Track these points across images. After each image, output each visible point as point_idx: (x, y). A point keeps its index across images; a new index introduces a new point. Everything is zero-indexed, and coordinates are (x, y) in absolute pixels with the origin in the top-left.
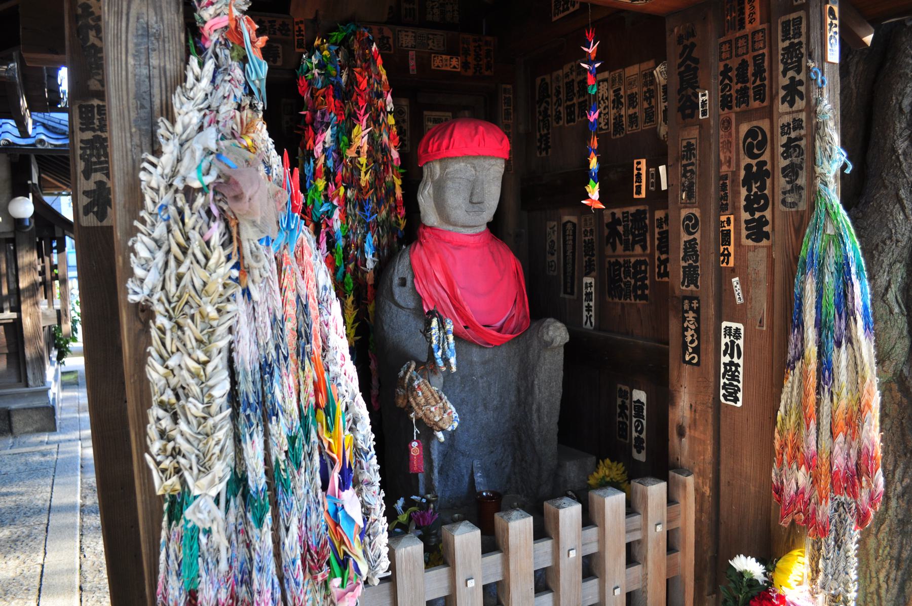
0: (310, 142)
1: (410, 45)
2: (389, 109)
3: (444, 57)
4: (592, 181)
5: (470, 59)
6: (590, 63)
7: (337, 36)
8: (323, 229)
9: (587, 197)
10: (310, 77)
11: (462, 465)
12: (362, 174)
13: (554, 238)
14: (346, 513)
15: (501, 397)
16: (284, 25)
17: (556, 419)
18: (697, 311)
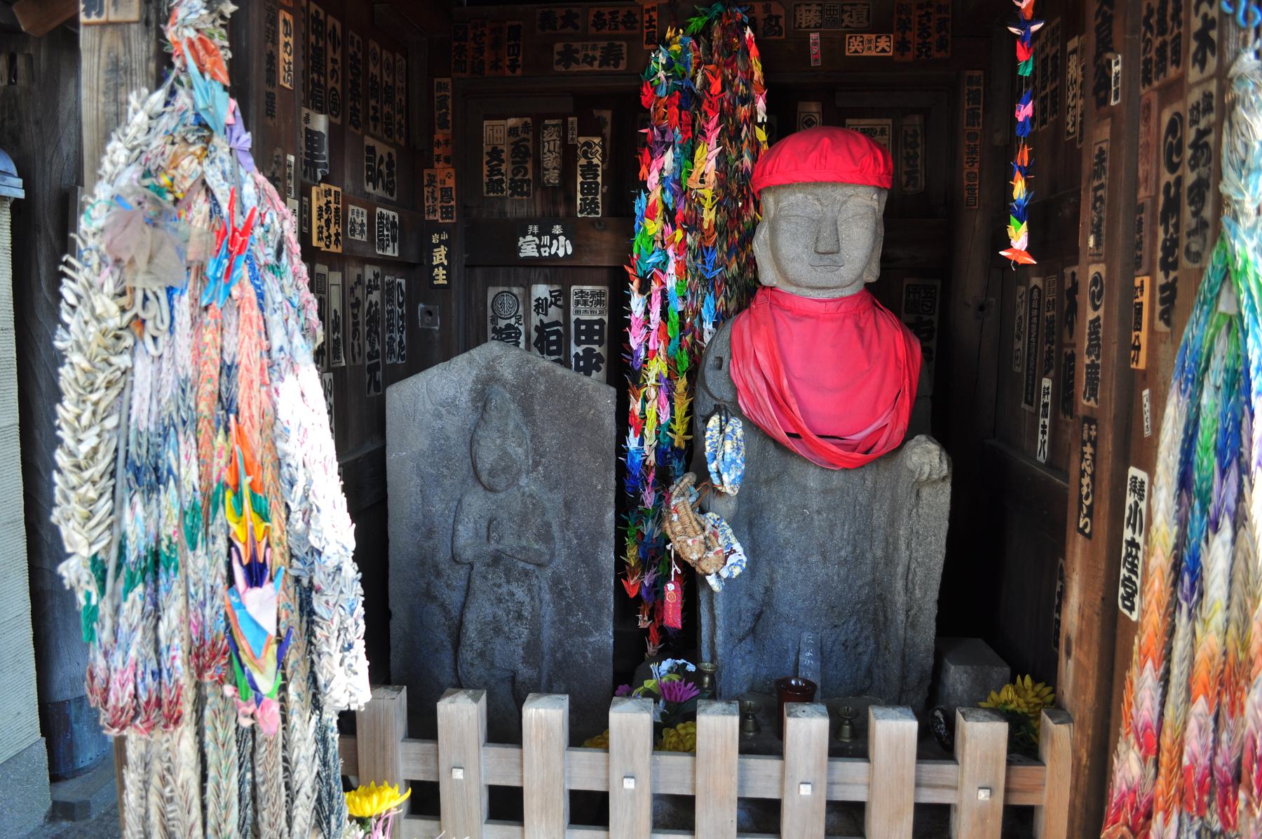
0: (644, 170)
1: (812, 24)
2: (760, 120)
3: (866, 36)
4: (1013, 219)
5: (909, 36)
6: (1024, 25)
7: (696, 23)
8: (655, 286)
9: (1007, 244)
10: (656, 82)
11: (785, 636)
12: (705, 212)
13: (1022, 312)
14: (247, 614)
15: (855, 547)
16: (630, 14)
17: (934, 594)
18: (1094, 445)
